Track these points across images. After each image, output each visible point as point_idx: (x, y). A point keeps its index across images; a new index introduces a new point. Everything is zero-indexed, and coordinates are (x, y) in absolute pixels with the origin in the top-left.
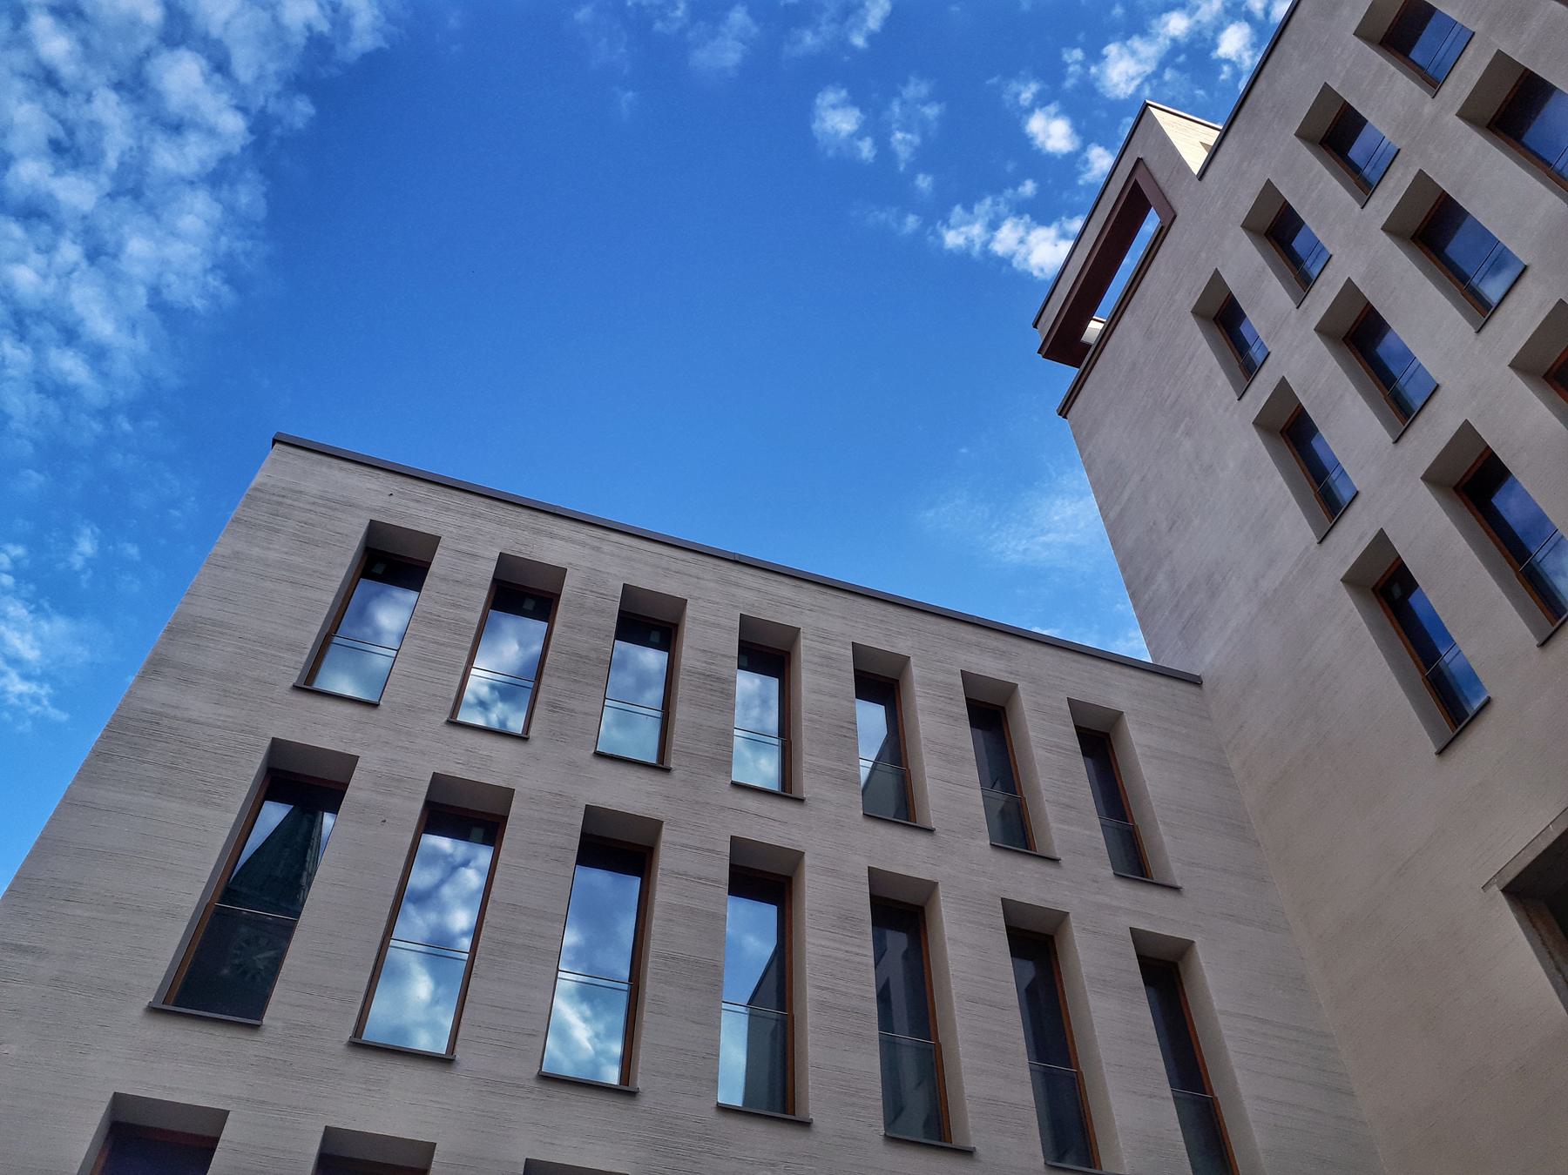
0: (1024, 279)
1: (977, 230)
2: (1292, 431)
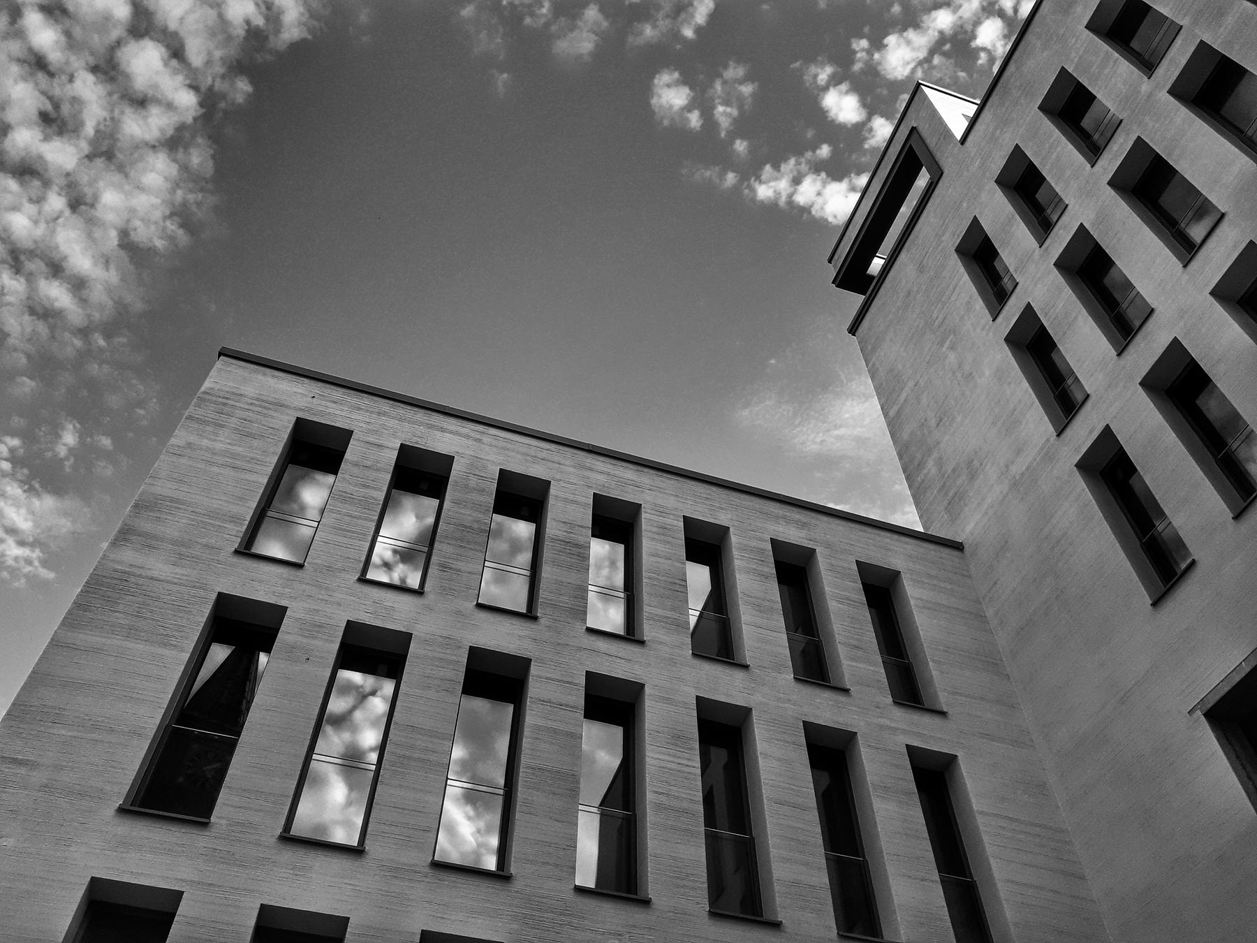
0: (821, 225)
1: (783, 185)
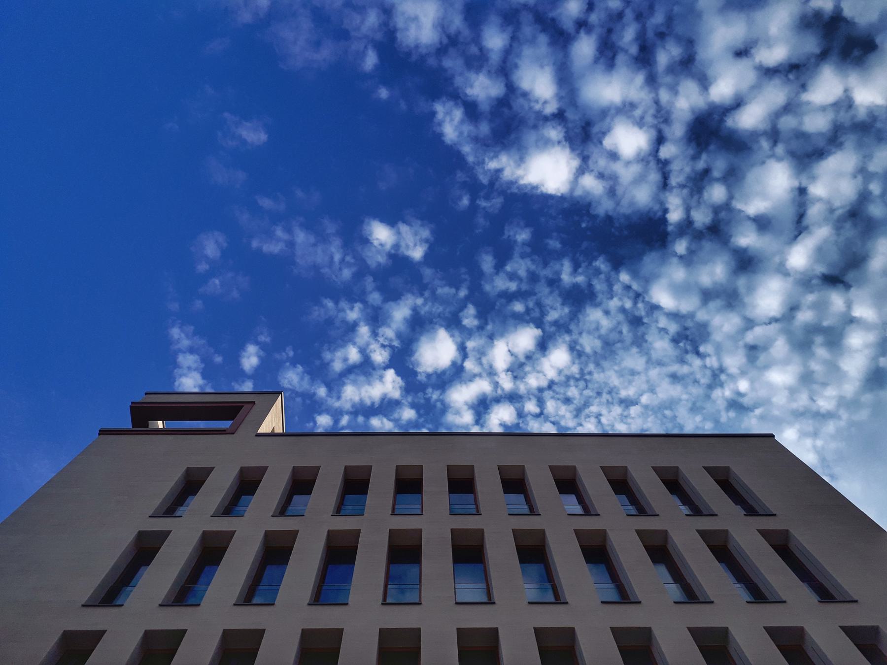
0: (171, 379)
1: (185, 343)
2: (145, 550)
